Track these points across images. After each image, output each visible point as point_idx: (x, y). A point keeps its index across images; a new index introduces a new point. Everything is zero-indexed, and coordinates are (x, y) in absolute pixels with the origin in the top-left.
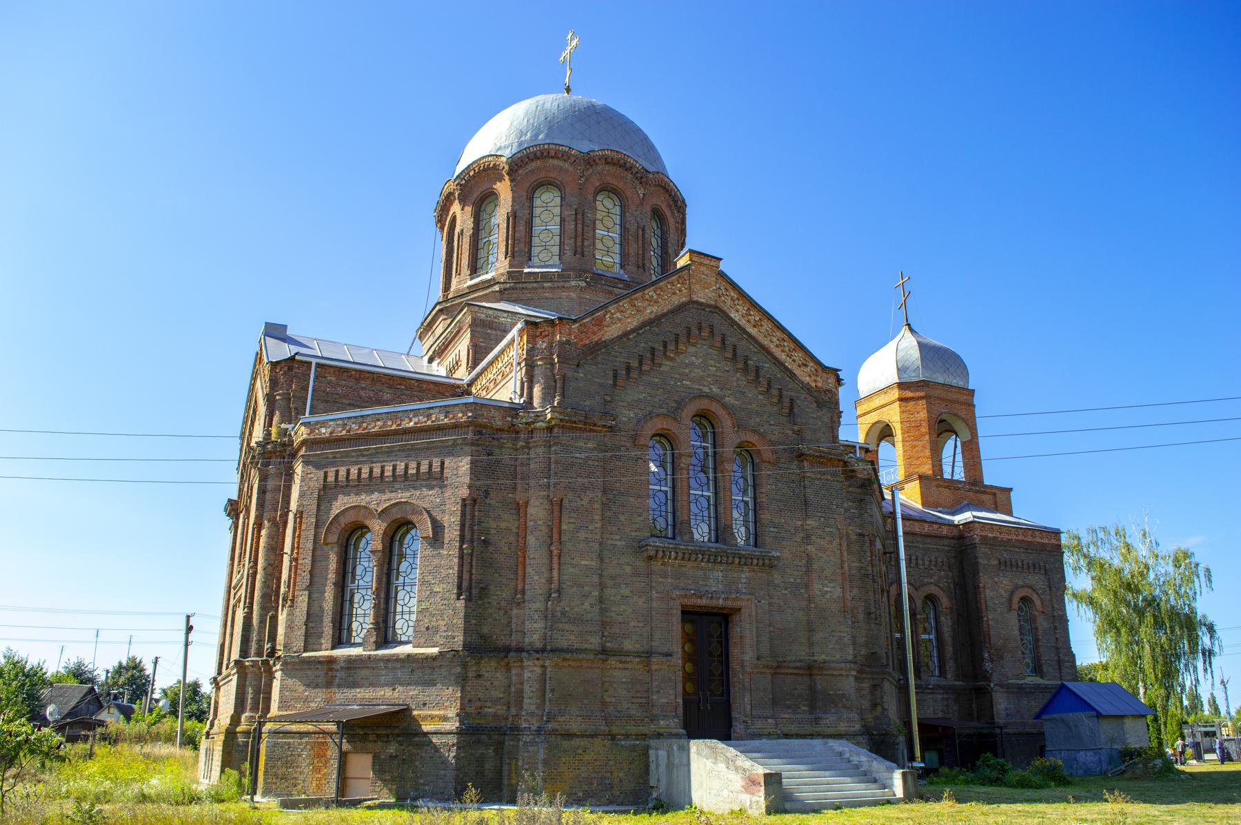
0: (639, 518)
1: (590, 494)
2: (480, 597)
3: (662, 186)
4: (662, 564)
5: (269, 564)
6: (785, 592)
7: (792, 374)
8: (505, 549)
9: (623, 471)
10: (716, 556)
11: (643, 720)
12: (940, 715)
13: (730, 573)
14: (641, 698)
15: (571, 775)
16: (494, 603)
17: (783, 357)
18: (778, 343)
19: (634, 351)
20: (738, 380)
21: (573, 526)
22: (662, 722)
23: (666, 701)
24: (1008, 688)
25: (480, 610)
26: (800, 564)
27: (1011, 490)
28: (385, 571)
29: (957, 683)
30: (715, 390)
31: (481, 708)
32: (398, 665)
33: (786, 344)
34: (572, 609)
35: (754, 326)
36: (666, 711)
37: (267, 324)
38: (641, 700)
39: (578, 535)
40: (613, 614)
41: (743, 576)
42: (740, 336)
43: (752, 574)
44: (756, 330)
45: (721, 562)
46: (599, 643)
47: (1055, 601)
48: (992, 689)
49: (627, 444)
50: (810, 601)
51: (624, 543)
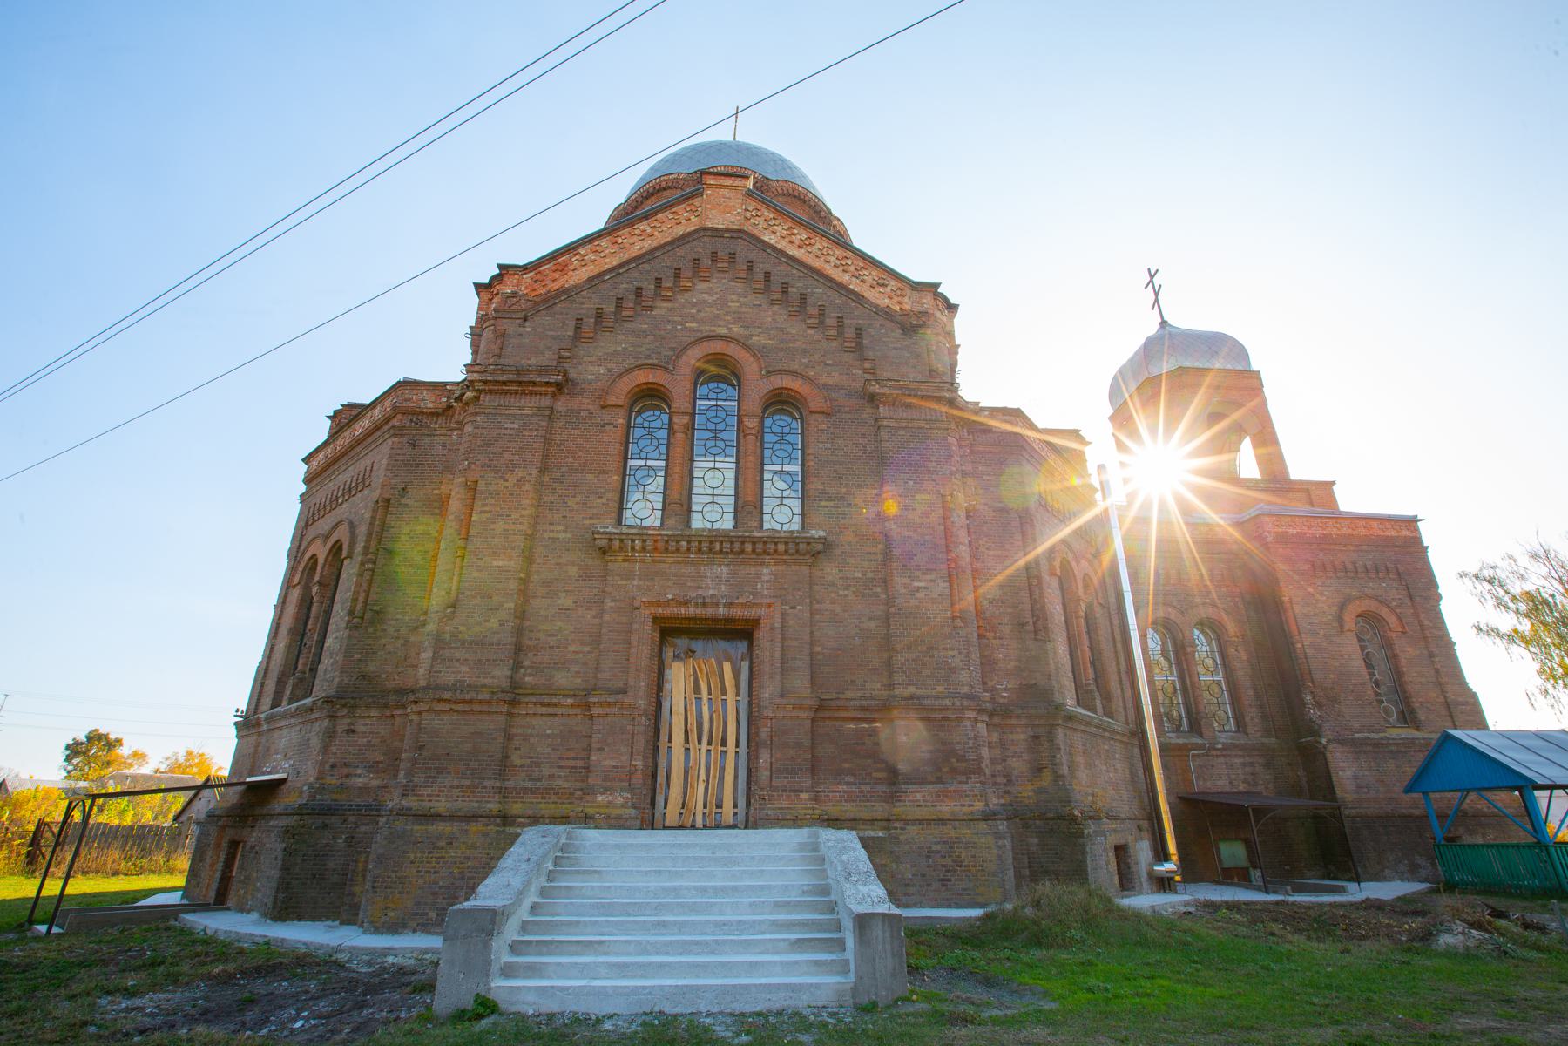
0: (600, 501)
1: (520, 473)
3: (795, 197)
4: (624, 561)
6: (846, 592)
7: (859, 297)
8: (418, 559)
9: (580, 441)
10: (711, 542)
11: (573, 794)
12: (1242, 787)
13: (742, 567)
14: (574, 759)
15: (421, 881)
16: (391, 630)
17: (845, 278)
18: (838, 262)
19: (612, 294)
20: (774, 314)
21: (488, 515)
22: (600, 798)
23: (612, 763)
24: (1357, 747)
26: (873, 550)
27: (1333, 483)
29: (1266, 740)
30: (735, 329)
31: (347, 776)
33: (849, 262)
34: (469, 629)
35: (800, 247)
36: (611, 780)
38: (571, 763)
39: (492, 526)
40: (541, 635)
41: (765, 571)
42: (777, 261)
43: (782, 568)
44: (803, 251)
45: (721, 551)
46: (507, 677)
47: (1422, 616)
48: (1324, 747)
49: (590, 407)
50: (889, 603)
51: (569, 536)
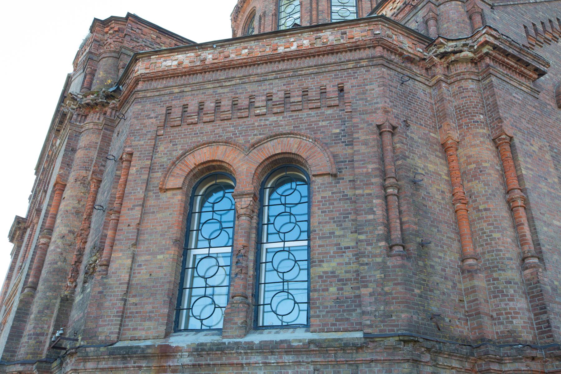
2: (420, 256)
5: (70, 232)
8: (438, 197)
25: (422, 276)
28: (255, 225)
32: (288, 359)
37: (128, 13)
